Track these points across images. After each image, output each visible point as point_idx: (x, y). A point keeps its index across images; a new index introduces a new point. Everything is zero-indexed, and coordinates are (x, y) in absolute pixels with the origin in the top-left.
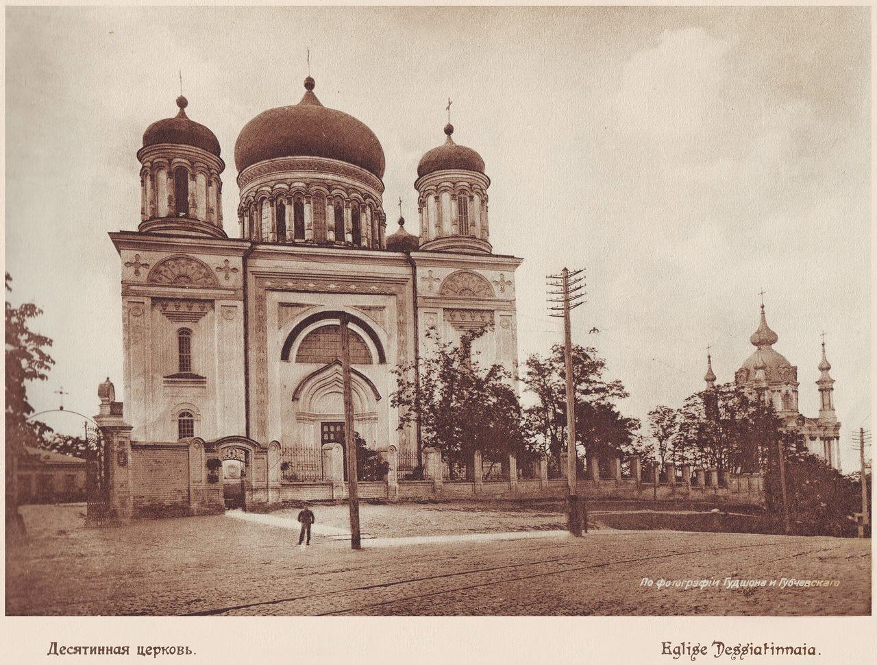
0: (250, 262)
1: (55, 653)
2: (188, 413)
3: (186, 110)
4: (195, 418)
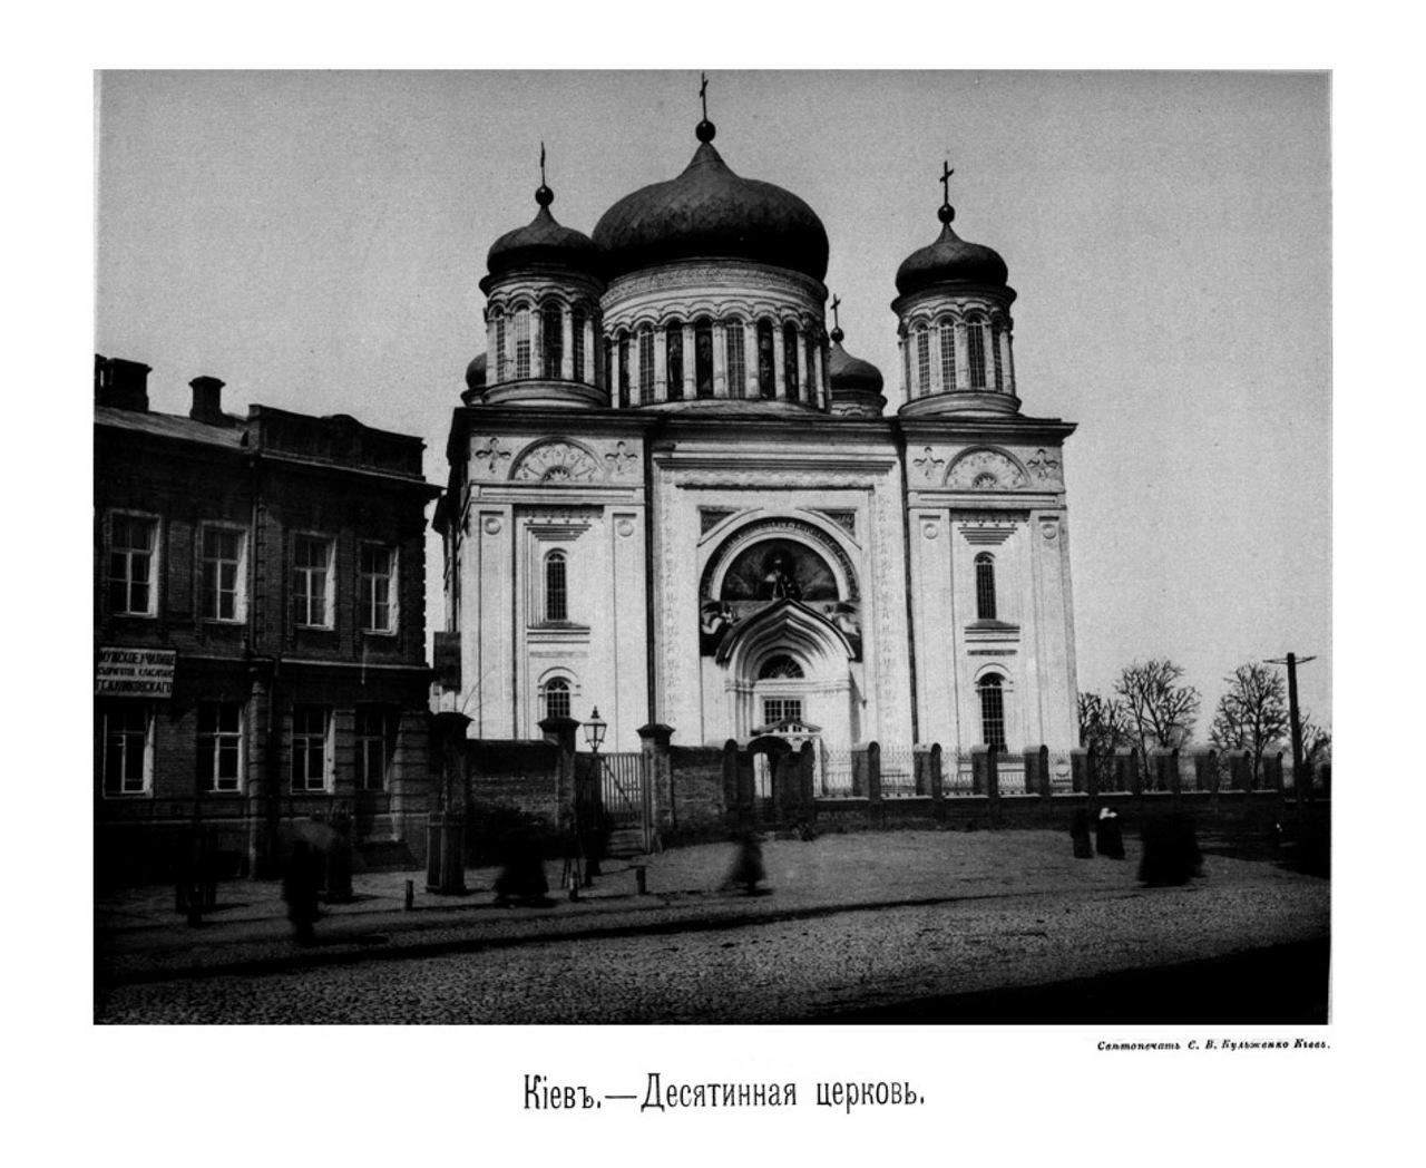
1: (659, 1105)
3: (953, 225)
4: (572, 690)
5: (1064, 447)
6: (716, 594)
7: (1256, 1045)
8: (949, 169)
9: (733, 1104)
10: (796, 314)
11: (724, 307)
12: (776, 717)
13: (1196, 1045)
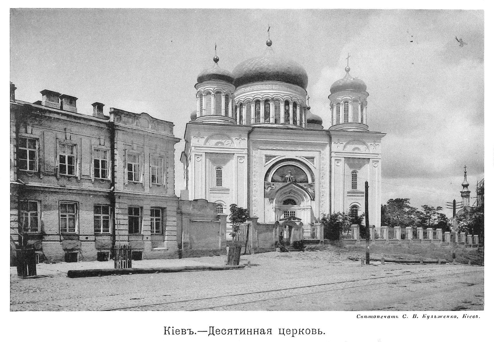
0: (251, 136)
2: (220, 205)
4: (224, 207)
5: (381, 140)
6: (269, 179)
7: (230, 331)
8: (347, 60)
9: (244, 334)
10: (297, 99)
11: (274, 96)
12: (287, 216)
13: (406, 316)
